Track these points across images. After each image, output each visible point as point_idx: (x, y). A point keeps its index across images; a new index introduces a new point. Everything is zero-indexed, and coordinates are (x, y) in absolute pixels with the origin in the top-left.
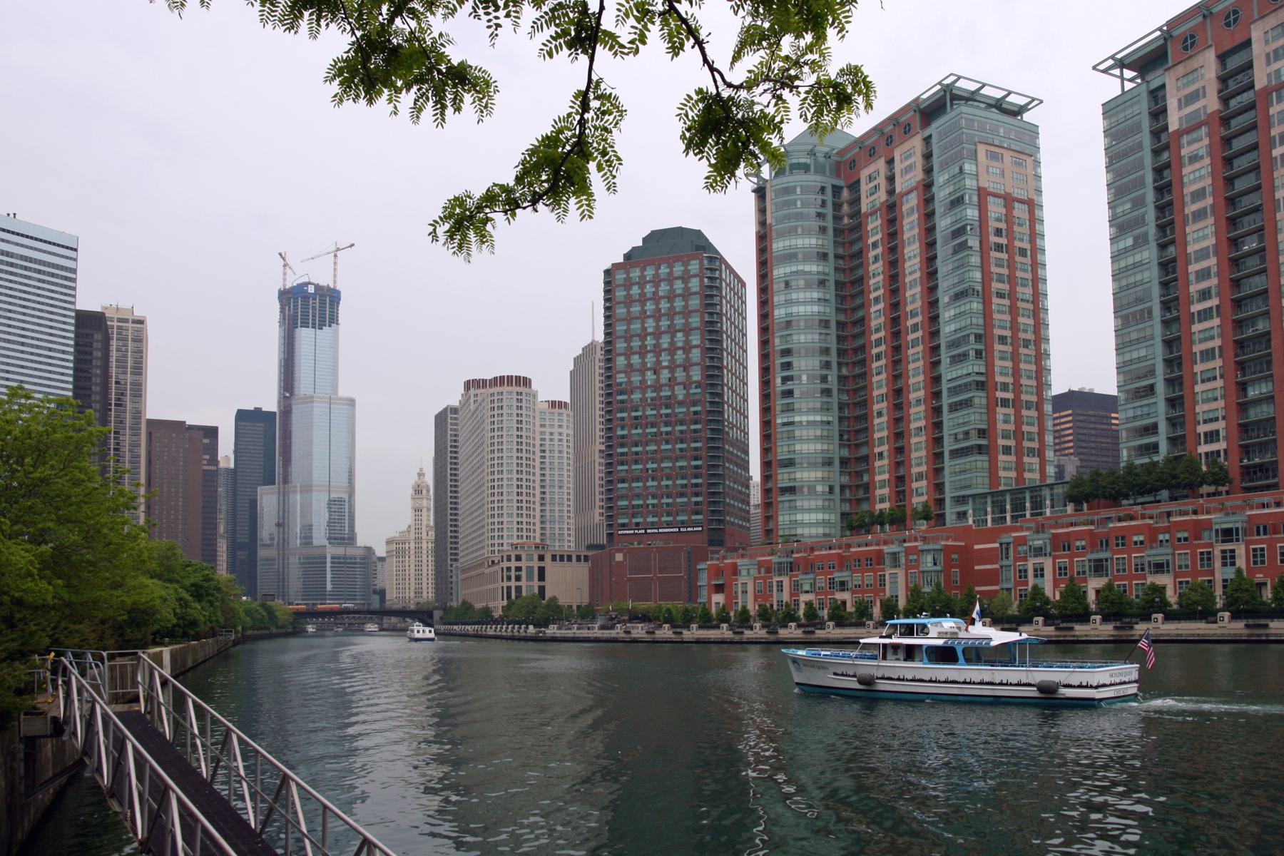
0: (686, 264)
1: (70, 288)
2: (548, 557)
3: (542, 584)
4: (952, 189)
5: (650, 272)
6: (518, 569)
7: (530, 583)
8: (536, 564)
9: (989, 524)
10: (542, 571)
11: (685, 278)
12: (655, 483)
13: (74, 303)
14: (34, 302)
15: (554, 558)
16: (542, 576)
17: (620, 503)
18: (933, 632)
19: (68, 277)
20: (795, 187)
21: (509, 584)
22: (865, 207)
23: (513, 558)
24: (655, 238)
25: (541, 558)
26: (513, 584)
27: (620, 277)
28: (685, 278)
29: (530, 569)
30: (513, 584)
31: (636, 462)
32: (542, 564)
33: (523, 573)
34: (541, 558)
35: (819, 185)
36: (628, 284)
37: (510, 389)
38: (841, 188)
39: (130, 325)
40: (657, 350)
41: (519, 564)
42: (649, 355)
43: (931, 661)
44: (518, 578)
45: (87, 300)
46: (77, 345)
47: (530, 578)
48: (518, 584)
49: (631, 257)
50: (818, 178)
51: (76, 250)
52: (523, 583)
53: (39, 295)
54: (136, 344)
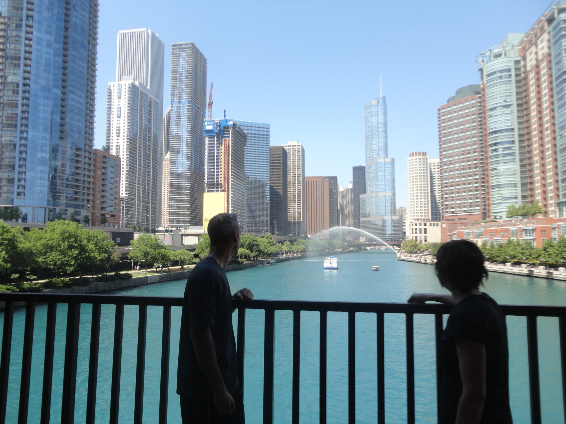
4: (510, 124)
6: (416, 229)
8: (423, 227)
10: (425, 230)
16: (425, 232)
19: (266, 137)
21: (421, 227)
22: (529, 68)
23: (414, 225)
25: (425, 225)
26: (414, 235)
30: (414, 235)
32: (425, 227)
33: (418, 231)
34: (425, 225)
39: (296, 147)
41: (416, 227)
43: (563, 211)
44: (416, 233)
45: (274, 143)
47: (421, 233)
52: (418, 235)
54: (86, 183)
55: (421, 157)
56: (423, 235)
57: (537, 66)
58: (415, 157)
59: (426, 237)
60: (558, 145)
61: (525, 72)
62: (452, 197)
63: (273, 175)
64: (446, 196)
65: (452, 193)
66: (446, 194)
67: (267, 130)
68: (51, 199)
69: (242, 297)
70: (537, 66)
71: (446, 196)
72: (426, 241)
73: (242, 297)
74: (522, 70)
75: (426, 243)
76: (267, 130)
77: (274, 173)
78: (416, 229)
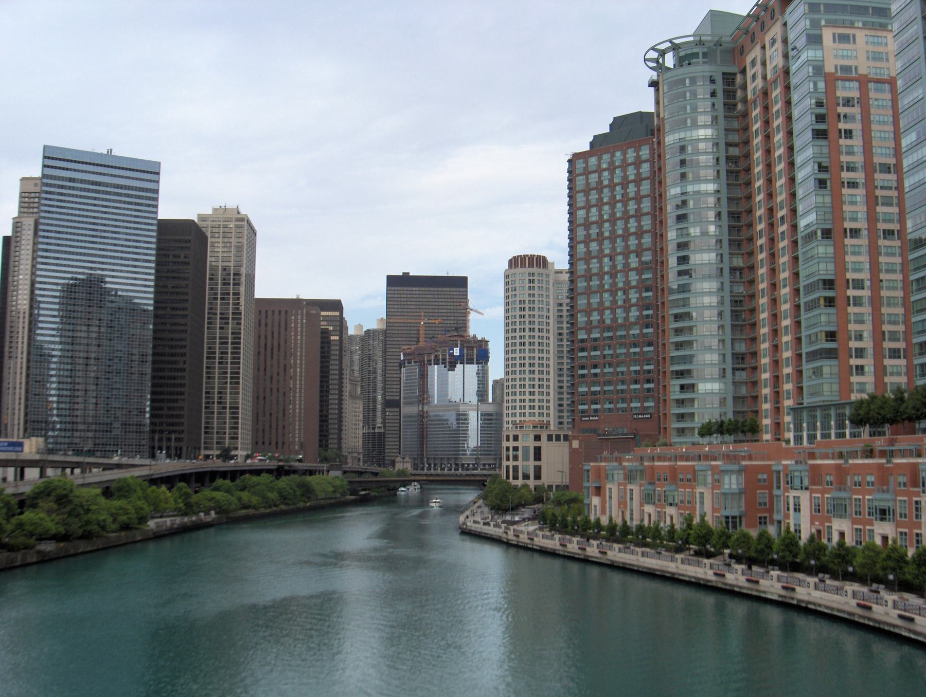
0: (638, 150)
1: (152, 212)
2: (544, 438)
3: (537, 463)
5: (631, 155)
7: (525, 463)
8: (532, 444)
9: (833, 438)
11: (638, 163)
12: (611, 370)
13: (156, 213)
14: (102, 218)
15: (550, 438)
17: (580, 390)
18: (26, 448)
20: (684, 80)
24: (619, 123)
25: (537, 438)
27: (580, 165)
28: (638, 163)
29: (526, 449)
31: (595, 349)
32: (538, 444)
33: (520, 453)
34: (537, 438)
35: (709, 74)
36: (587, 172)
37: (523, 270)
38: (735, 74)
40: (600, 238)
42: (632, 238)
44: (516, 458)
46: (159, 241)
47: (526, 458)
48: (515, 463)
49: (598, 143)
50: (707, 68)
51: (158, 174)
53: (106, 213)
55: (535, 270)
56: (532, 463)
57: (765, 93)
58: (520, 270)
59: (538, 470)
60: (802, 274)
61: (745, 100)
62: (596, 375)
63: (160, 416)
64: (581, 372)
65: (595, 367)
66: (583, 368)
67: (154, 210)
68: (39, 530)
69: (473, 440)
70: (765, 93)
71: (581, 372)
72: (538, 476)
73: (473, 440)
74: (739, 94)
75: (538, 483)
76: (154, 210)
77: (165, 412)
78: (516, 449)
